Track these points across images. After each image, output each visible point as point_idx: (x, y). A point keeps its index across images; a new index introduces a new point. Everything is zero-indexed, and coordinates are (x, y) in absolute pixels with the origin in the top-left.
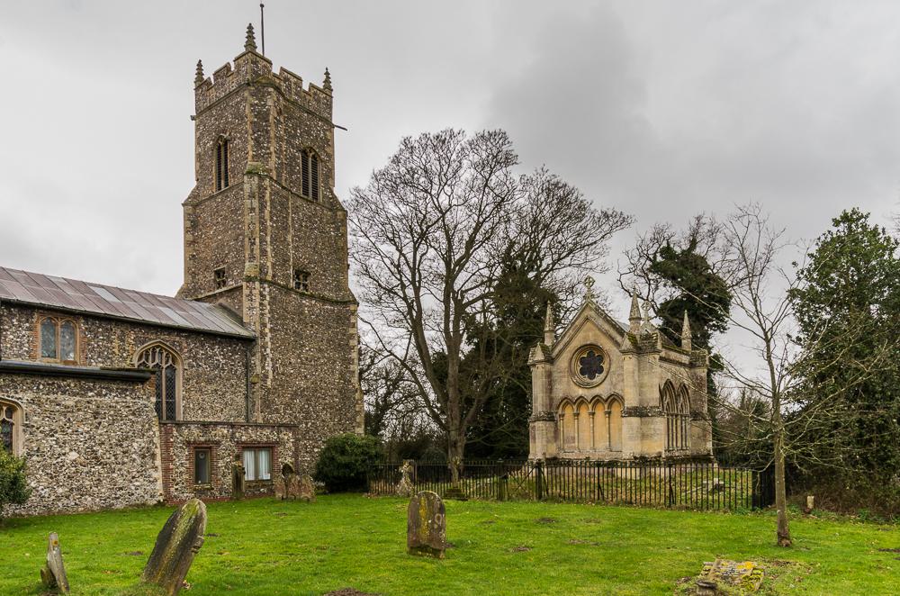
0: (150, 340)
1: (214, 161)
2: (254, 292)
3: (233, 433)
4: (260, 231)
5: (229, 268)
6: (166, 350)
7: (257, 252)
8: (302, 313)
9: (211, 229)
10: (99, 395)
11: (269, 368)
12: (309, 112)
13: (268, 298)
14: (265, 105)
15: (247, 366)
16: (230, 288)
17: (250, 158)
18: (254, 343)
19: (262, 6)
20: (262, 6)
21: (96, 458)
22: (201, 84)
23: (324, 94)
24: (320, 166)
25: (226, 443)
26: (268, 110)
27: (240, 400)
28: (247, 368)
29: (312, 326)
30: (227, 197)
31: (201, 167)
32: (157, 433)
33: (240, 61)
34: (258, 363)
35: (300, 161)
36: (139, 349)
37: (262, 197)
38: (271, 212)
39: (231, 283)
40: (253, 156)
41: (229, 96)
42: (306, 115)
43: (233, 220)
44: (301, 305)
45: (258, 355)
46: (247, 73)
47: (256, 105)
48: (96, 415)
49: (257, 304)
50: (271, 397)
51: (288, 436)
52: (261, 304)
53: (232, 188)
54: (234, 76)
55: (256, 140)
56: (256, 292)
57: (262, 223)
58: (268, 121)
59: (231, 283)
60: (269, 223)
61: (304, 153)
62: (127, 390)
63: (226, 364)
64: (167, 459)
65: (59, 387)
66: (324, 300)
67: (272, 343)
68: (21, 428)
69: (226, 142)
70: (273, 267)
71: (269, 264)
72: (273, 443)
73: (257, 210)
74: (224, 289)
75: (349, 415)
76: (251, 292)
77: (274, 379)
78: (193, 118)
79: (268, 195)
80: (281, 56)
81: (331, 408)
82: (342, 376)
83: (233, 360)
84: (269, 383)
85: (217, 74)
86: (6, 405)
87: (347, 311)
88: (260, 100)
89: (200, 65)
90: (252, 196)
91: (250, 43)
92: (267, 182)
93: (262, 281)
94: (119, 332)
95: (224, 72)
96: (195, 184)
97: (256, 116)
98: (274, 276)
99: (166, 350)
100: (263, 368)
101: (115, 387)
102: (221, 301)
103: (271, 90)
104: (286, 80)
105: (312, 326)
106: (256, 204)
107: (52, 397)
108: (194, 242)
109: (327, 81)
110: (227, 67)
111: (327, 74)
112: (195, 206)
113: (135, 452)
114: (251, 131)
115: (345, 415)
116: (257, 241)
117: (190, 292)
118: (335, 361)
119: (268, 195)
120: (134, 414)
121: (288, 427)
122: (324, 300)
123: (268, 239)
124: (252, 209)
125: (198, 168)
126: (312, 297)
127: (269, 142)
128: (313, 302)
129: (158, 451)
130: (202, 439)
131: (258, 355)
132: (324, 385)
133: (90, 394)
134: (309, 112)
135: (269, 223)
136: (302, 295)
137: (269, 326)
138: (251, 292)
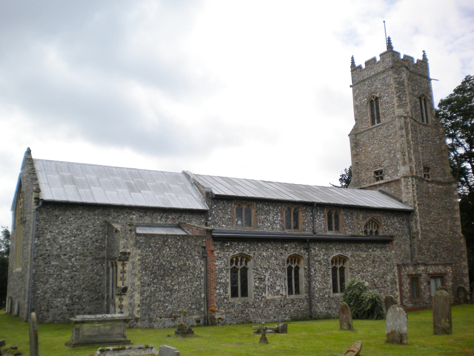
0: (368, 217)
1: (369, 109)
2: (409, 183)
3: (426, 269)
4: (408, 147)
5: (385, 169)
6: (375, 222)
7: (407, 160)
8: (428, 193)
9: (370, 147)
10: (373, 251)
11: (419, 228)
12: (419, 75)
13: (415, 186)
14: (401, 78)
15: (410, 228)
16: (386, 181)
17: (396, 107)
18: (412, 213)
19: (384, 22)
20: (384, 22)
21: (375, 285)
22: (355, 69)
23: (424, 63)
24: (428, 104)
25: (424, 275)
26: (404, 80)
27: (408, 248)
28: (409, 229)
29: (434, 200)
30: (381, 129)
31: (358, 112)
32: (397, 271)
33: (384, 56)
34: (414, 225)
35: (418, 103)
36: (364, 223)
37: (407, 129)
38: (412, 136)
39: (387, 178)
40: (398, 106)
41: (378, 74)
42: (418, 77)
43: (386, 142)
44: (428, 188)
45: (414, 221)
46: (389, 62)
47: (397, 78)
48: (373, 261)
49: (411, 191)
50: (422, 245)
51: (449, 269)
52: (413, 190)
53: (383, 125)
54: (380, 63)
55: (399, 97)
56: (409, 183)
57: (408, 143)
58: (404, 86)
59: (387, 178)
60: (412, 143)
61: (420, 98)
62: (383, 247)
63: (400, 227)
64: (401, 285)
65: (360, 248)
66: (439, 183)
67: (419, 213)
68: (349, 270)
69: (377, 99)
70: (416, 168)
71: (414, 166)
72: (443, 274)
73: (405, 136)
74: (382, 182)
75: (458, 254)
76: (407, 184)
77: (422, 235)
78: (351, 86)
79: (409, 127)
80: (403, 50)
81: (447, 250)
82: (451, 229)
83: (403, 225)
84: (420, 237)
85: (367, 63)
86: (343, 258)
87: (451, 188)
88: (399, 75)
89: (352, 58)
90: (401, 128)
91: (389, 46)
92: (408, 120)
93: (412, 177)
94: (356, 214)
95: (371, 63)
96: (354, 123)
97: (397, 84)
98: (416, 172)
99: (375, 222)
100: (416, 228)
101: (378, 246)
102: (381, 188)
103: (404, 68)
104: (407, 60)
105: (434, 200)
106: (404, 132)
107: (358, 253)
108: (357, 155)
109: (424, 56)
110: (374, 59)
111: (424, 51)
112: (356, 135)
113: (389, 281)
114: (395, 93)
115: (455, 254)
116: (407, 153)
117: (348, 181)
118: (447, 220)
119: (409, 127)
120: (387, 260)
121: (450, 264)
122: (439, 183)
123: (412, 151)
124: (402, 136)
125: (356, 113)
126: (433, 182)
127: (406, 97)
128: (433, 185)
129: (397, 280)
130: (414, 273)
131: (414, 221)
132: (442, 235)
133: (370, 250)
134: (419, 75)
135: (412, 143)
136: (428, 182)
137: (417, 202)
138: (407, 184)
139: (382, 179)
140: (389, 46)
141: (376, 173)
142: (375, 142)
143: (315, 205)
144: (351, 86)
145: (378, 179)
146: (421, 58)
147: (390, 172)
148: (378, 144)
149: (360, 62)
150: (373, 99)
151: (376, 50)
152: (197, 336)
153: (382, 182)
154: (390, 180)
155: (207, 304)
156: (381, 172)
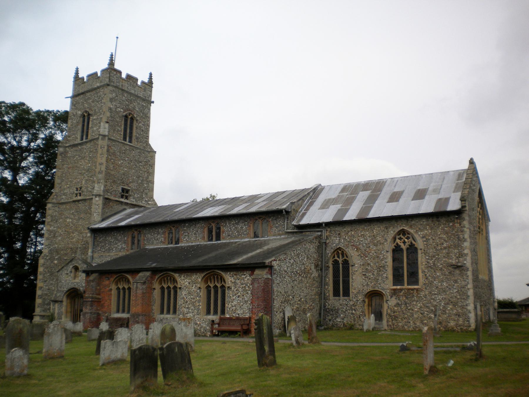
19: (117, 38)
20: (117, 38)
39: (132, 200)
59: (132, 200)
74: (126, 201)
78: (153, 102)
80: (125, 67)
85: (89, 76)
91: (112, 63)
95: (93, 76)
110: (96, 74)
139: (127, 198)
140: (112, 63)
141: (123, 190)
142: (126, 159)
143: (324, 225)
144: (153, 102)
145: (122, 197)
146: (146, 80)
147: (136, 196)
148: (129, 163)
149: (84, 74)
150: (86, 114)
151: (99, 66)
152: (369, 309)
153: (126, 201)
154: (135, 203)
155: (322, 281)
156: (128, 191)
